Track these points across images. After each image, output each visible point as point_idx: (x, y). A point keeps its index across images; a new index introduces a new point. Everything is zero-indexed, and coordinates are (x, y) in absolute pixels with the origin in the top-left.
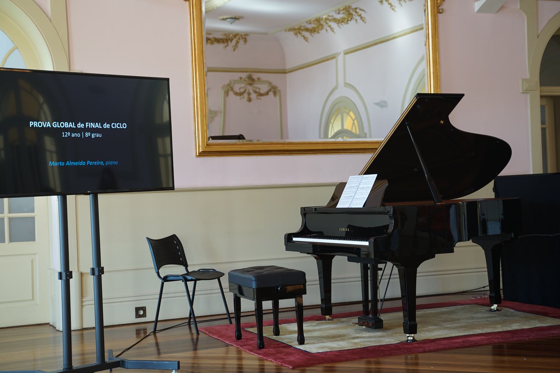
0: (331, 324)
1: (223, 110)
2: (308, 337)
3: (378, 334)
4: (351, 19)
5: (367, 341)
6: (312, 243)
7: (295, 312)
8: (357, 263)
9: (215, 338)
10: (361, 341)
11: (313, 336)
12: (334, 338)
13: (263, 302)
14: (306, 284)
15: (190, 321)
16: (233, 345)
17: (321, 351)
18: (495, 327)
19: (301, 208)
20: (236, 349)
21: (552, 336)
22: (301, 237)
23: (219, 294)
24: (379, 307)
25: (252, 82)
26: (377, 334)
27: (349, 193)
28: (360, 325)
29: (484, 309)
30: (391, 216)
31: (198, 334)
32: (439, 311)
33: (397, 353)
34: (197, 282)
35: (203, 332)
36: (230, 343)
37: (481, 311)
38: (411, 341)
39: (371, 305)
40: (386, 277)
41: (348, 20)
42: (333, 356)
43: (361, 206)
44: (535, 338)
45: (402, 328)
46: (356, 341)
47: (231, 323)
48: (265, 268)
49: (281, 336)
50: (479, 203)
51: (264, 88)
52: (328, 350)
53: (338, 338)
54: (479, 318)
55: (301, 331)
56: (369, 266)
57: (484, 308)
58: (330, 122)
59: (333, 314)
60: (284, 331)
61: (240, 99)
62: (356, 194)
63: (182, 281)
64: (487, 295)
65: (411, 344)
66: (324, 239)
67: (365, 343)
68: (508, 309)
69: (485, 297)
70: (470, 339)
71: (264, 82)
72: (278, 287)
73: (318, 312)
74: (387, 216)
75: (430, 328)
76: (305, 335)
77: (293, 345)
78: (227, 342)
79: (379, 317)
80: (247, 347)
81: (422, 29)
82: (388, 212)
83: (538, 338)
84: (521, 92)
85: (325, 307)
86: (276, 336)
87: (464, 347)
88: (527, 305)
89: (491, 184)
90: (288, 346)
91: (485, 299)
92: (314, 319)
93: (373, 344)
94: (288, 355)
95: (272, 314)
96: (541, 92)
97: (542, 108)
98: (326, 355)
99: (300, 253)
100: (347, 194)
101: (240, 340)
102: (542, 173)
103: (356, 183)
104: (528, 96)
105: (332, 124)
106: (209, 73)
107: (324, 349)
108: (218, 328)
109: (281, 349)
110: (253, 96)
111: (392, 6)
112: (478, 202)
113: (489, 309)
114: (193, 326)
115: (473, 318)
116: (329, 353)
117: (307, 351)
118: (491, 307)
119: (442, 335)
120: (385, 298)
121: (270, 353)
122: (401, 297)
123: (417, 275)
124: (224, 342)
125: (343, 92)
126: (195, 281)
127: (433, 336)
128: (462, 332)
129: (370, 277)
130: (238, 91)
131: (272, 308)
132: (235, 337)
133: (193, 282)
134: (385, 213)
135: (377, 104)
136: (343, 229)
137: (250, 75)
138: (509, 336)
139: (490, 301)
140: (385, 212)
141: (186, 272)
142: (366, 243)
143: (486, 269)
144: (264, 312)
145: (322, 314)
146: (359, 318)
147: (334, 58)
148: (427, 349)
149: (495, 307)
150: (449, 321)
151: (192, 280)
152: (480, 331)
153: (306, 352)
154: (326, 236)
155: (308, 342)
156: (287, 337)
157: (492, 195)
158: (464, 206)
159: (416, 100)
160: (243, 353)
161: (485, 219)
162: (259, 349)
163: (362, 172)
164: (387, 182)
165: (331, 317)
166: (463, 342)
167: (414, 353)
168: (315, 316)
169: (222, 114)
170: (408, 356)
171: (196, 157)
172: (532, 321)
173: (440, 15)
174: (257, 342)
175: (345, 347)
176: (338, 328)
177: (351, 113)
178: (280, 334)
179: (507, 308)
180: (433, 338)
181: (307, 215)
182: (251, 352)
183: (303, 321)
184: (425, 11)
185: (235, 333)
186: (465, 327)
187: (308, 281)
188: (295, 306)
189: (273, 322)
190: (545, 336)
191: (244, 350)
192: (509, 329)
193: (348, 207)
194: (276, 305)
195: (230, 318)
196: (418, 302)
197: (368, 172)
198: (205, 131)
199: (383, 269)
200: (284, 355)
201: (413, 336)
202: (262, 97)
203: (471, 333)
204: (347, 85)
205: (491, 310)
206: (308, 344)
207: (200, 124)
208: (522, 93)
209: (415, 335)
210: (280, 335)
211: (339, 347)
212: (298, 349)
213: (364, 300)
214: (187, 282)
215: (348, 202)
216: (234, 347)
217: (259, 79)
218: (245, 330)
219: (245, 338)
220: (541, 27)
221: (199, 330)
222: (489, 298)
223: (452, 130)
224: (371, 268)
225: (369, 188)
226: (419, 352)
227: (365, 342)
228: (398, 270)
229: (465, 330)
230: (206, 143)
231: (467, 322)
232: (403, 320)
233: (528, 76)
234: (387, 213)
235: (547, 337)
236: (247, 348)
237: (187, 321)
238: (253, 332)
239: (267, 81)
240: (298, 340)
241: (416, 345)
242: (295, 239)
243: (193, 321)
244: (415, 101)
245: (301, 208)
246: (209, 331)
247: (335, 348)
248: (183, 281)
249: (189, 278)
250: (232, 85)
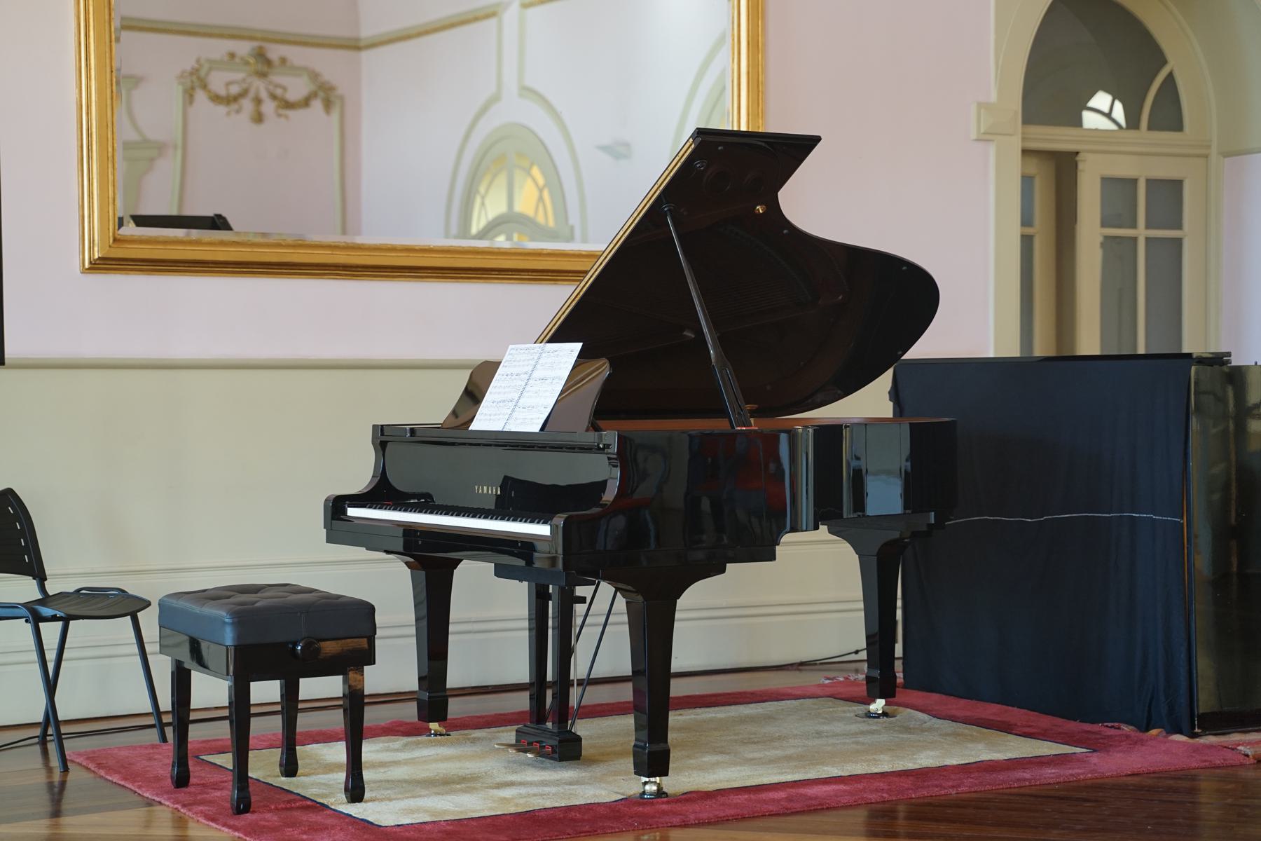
0: (443, 746)
1: (180, 143)
2: (375, 782)
3: (567, 773)
5: (535, 795)
6: (403, 526)
7: (341, 711)
8: (521, 581)
9: (114, 781)
10: (520, 794)
11: (390, 778)
12: (446, 784)
13: (252, 684)
14: (376, 636)
15: (45, 734)
16: (163, 801)
17: (406, 821)
18: (874, 759)
19: (374, 426)
20: (173, 813)
21: (1016, 785)
22: (370, 507)
23: (134, 657)
24: (573, 701)
25: (265, 69)
26: (563, 775)
27: (507, 390)
28: (519, 750)
29: (849, 711)
30: (614, 459)
31: (66, 769)
32: (733, 714)
33: (612, 828)
34: (72, 623)
35: (80, 764)
36: (153, 798)
37: (843, 715)
38: (650, 795)
39: (553, 695)
40: (596, 619)
42: (440, 835)
43: (535, 428)
44: (973, 790)
45: (631, 759)
46: (507, 793)
47: (164, 739)
48: (262, 591)
49: (302, 778)
50: (848, 429)
51: (297, 88)
52: (428, 819)
53: (458, 783)
54: (836, 735)
55: (355, 764)
56: (551, 591)
57: (850, 709)
58: (477, 192)
59: (449, 717)
60: (310, 764)
61: (228, 114)
62: (525, 394)
63: (24, 619)
64: (862, 674)
65: (652, 804)
66: (431, 513)
67: (529, 799)
68: (912, 711)
69: (856, 677)
70: (808, 790)
71: (297, 71)
72: (295, 644)
73: (409, 712)
74: (605, 457)
75: (704, 759)
76: (367, 775)
77: (332, 804)
78: (147, 795)
79: (573, 731)
80: (201, 808)
82: (607, 446)
83: (981, 791)
84: (975, 137)
85: (429, 697)
86: (286, 776)
87: (789, 811)
88: (963, 702)
90: (318, 805)
91: (855, 683)
92: (398, 731)
93: (549, 804)
94: (316, 830)
95: (280, 717)
96: (1024, 139)
97: (1027, 181)
98: (420, 831)
99: (367, 549)
100: (499, 393)
101: (184, 789)
102: (1018, 355)
103: (523, 366)
104: (992, 149)
105: (483, 198)
106: (125, 35)
107: (415, 816)
108: (124, 753)
109: (296, 814)
110: (269, 107)
112: (846, 427)
113: (866, 711)
114: (52, 747)
115: (819, 734)
116: (428, 827)
117: (370, 819)
118: (869, 704)
119: (735, 781)
120: (591, 677)
121: (264, 826)
122: (631, 674)
124: (139, 794)
125: (514, 110)
126: (66, 620)
127: (711, 783)
128: (789, 773)
129: (553, 618)
130: (223, 92)
131: (279, 700)
132: (170, 780)
133: (60, 624)
134: (599, 450)
135: (605, 149)
136: (485, 488)
137: (261, 48)
138: (906, 786)
139: (867, 688)
140: (598, 445)
141: (39, 596)
142: (543, 530)
143: (861, 605)
144: (253, 710)
145: (419, 720)
146: (517, 731)
147: (493, 14)
148: (692, 817)
149: (878, 705)
150: (758, 742)
151: (54, 618)
152: (834, 771)
153: (365, 825)
154: (438, 505)
155: (374, 795)
156: (318, 781)
157: (885, 409)
158: (808, 435)
159: (693, 146)
160: (191, 824)
161: (861, 470)
162: (235, 814)
163: (543, 336)
164: (608, 367)
165: (445, 727)
166: (789, 799)
167: (658, 827)
168: (401, 724)
169: (179, 153)
170: (642, 838)
171: (82, 273)
172: (970, 745)
174: (230, 793)
175: (473, 812)
176: (459, 758)
177: (536, 171)
178: (299, 771)
179: (909, 710)
180: (711, 788)
181: (389, 446)
182: (211, 824)
183: (364, 738)
185: (170, 768)
186: (800, 758)
187: (380, 628)
188: (341, 695)
189: (281, 737)
190: (999, 785)
191: (193, 818)
192: (910, 766)
193: (501, 429)
194: (290, 693)
195: (161, 726)
196: (678, 688)
197: (560, 335)
198: (111, 200)
199: (588, 601)
200: (305, 833)
201: (658, 781)
202: (290, 113)
203: (812, 775)
204: (527, 91)
205: (869, 715)
206: (372, 800)
207: (95, 181)
209: (664, 778)
210: (299, 776)
211: (456, 809)
212: (344, 814)
213: (533, 680)
214: (40, 624)
215: (501, 416)
216: (165, 808)
217: (283, 61)
218: (203, 760)
219: (199, 782)
221: (67, 757)
222: (865, 682)
223: (785, 231)
224: (556, 597)
225: (560, 378)
226: (671, 826)
227: (528, 795)
228: (627, 603)
229: (795, 766)
230: (111, 234)
231: (804, 746)
232: (634, 738)
233: (993, 97)
234: (603, 449)
235: (1003, 789)
236: (202, 812)
237: (37, 732)
238: (221, 766)
239: (305, 69)
240: (346, 790)
241: (665, 807)
242: (352, 512)
243: (51, 733)
244: (690, 150)
245: (374, 426)
246: (98, 761)
247: (445, 812)
248: (27, 621)
249: (46, 611)
250: (203, 73)
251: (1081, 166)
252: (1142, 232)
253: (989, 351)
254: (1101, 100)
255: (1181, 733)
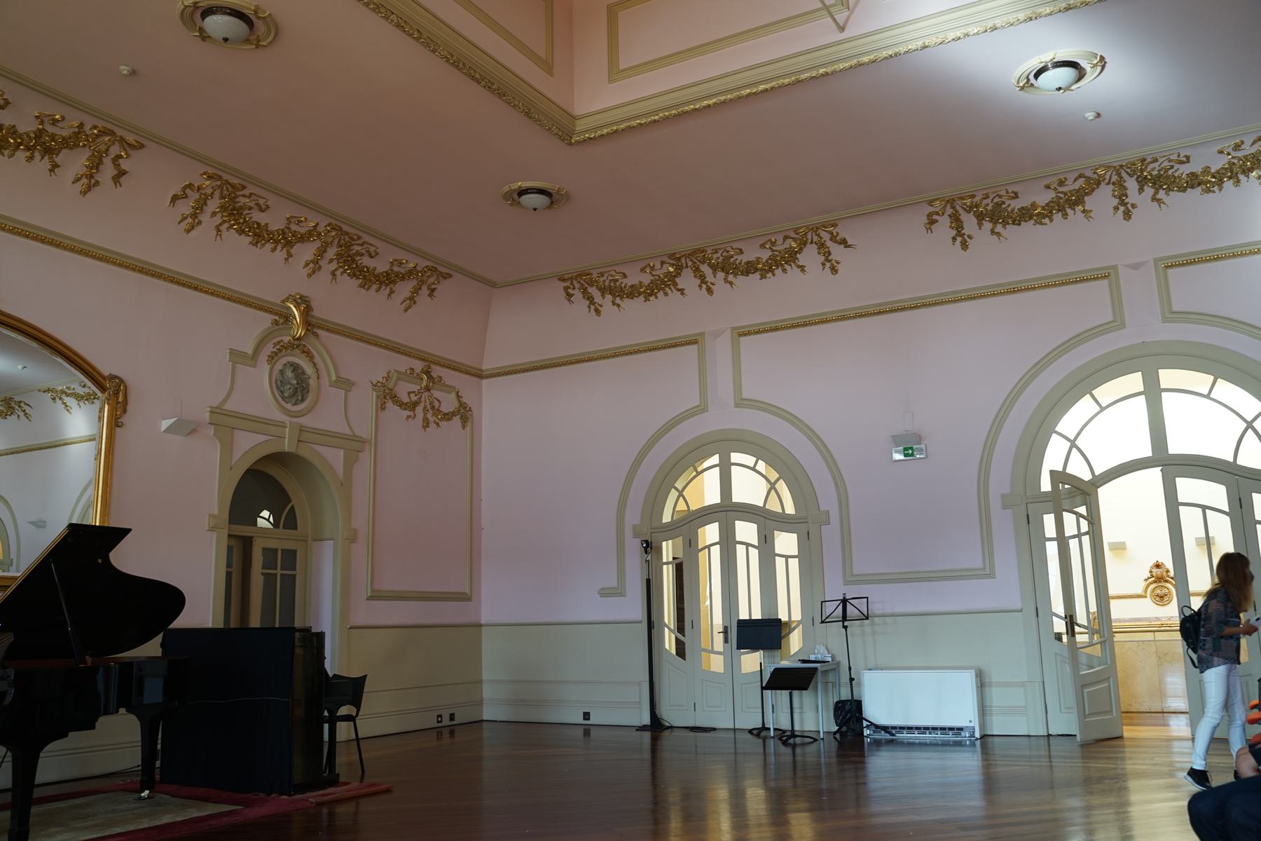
4: (12, 413)
41: (6, 415)
51: (449, 403)
71: (449, 389)
81: (94, 440)
82: (8, 677)
89: (159, 638)
96: (229, 530)
97: (230, 549)
104: (215, 535)
111: (67, 406)
123: (140, 744)
135: (32, 523)
157: (158, 652)
173: (118, 429)
184: (99, 418)
192: (158, 823)
203: (107, 833)
205: (141, 798)
208: (208, 530)
220: (235, 459)
233: (216, 512)
251: (254, 543)
252: (279, 572)
253: (210, 624)
254: (265, 514)
255: (285, 795)
